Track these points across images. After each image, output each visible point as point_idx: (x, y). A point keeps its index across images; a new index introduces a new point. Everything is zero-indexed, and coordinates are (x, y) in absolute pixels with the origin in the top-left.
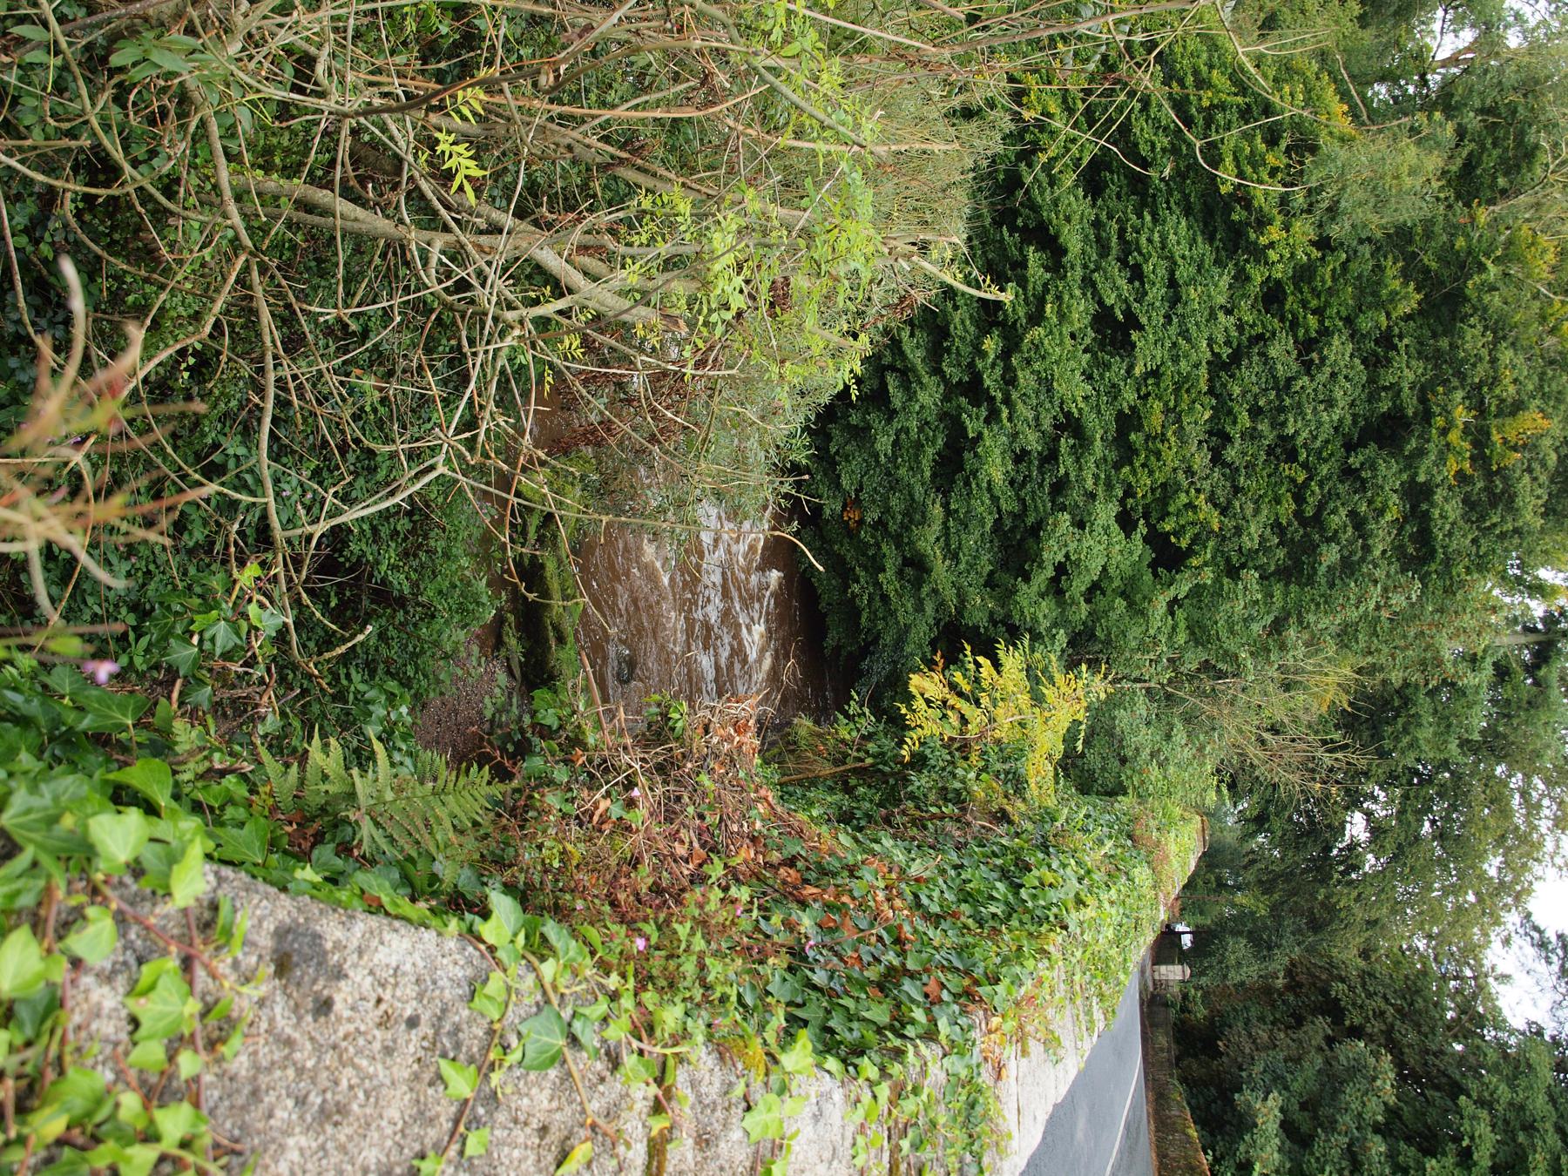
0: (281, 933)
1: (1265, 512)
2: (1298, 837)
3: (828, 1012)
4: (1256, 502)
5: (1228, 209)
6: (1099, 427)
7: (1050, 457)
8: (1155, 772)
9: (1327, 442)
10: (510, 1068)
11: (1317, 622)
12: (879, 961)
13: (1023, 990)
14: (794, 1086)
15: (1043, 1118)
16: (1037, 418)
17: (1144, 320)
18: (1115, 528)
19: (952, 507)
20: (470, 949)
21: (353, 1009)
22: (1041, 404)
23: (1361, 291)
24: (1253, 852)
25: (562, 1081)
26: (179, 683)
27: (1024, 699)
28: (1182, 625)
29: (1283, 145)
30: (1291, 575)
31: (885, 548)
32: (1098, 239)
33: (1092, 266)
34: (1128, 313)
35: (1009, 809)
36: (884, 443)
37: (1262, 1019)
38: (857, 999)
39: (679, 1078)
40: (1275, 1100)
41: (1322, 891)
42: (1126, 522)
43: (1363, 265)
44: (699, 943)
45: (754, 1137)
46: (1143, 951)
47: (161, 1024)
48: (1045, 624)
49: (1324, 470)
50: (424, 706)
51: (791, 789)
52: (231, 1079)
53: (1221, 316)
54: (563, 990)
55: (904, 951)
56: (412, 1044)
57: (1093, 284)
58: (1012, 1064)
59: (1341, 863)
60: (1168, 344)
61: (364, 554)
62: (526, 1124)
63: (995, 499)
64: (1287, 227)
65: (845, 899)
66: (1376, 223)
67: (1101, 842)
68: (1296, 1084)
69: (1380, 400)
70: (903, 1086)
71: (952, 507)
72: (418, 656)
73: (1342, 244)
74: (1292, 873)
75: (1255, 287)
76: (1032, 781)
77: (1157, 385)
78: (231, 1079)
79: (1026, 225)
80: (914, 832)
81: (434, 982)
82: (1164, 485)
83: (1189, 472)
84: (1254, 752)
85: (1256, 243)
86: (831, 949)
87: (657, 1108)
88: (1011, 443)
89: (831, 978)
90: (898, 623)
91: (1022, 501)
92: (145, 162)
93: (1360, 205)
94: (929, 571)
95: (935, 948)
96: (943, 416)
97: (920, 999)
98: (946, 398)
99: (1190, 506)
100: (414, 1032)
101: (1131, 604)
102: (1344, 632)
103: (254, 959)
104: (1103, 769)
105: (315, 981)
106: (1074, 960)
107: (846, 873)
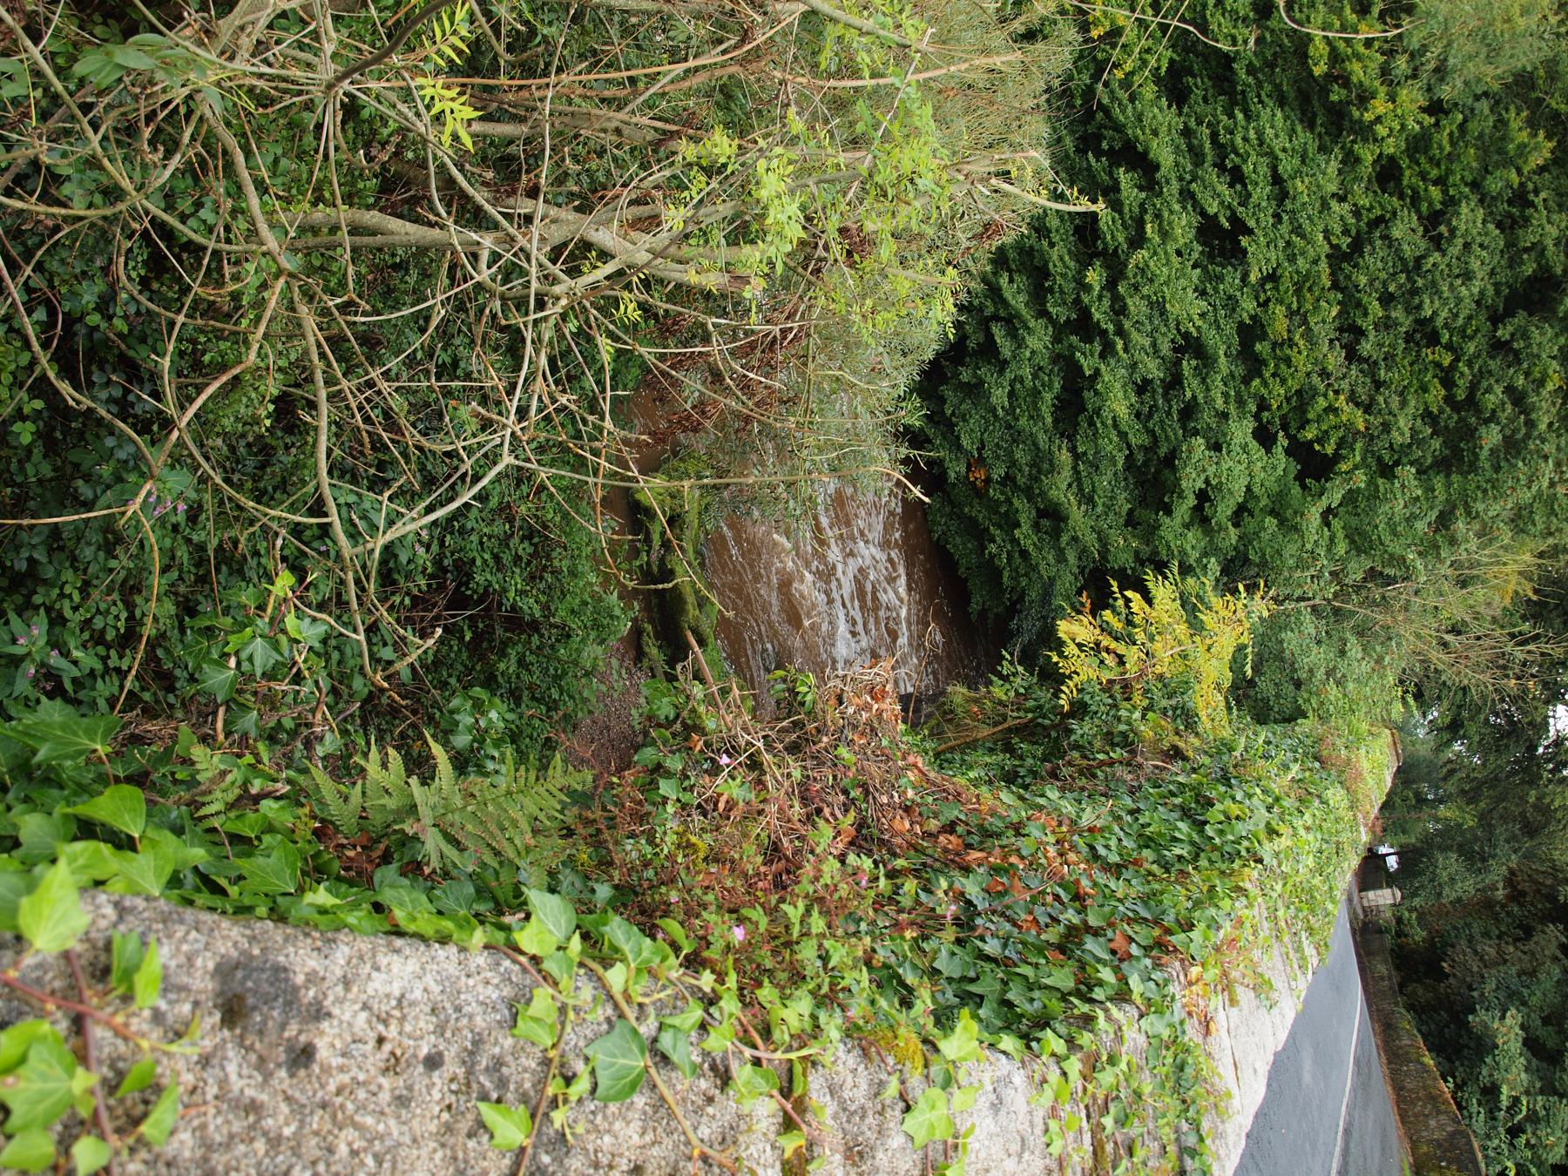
0: (224, 971)
1: (1413, 403)
2: (1498, 740)
3: (1005, 983)
4: (1401, 394)
5: (1325, 92)
6: (1220, 344)
7: (1174, 382)
8: (1333, 691)
9: (1470, 318)
10: (580, 1101)
11: (1486, 511)
12: (1058, 921)
13: (1222, 933)
14: (962, 1076)
15: (1264, 1068)
16: (1154, 345)
17: (1251, 223)
18: (1253, 445)
19: (1080, 450)
20: (507, 963)
21: (344, 1055)
22: (1156, 330)
23: (1484, 150)
24: (1450, 761)
25: (656, 1109)
26: (221, 711)
27: (1182, 629)
28: (1340, 534)
29: (1376, 11)
30: (1451, 465)
31: (1016, 501)
32: (1191, 148)
33: (1188, 177)
34: (1234, 219)
35: (1181, 745)
36: (999, 396)
37: (1486, 934)
38: (1036, 966)
39: (814, 1086)
40: (1513, 1018)
41: (1533, 792)
42: (1264, 437)
43: (1484, 121)
44: (818, 923)
45: (919, 1141)
46: (1349, 876)
47: (41, 1108)
48: (1194, 555)
49: (1471, 348)
50: (575, 727)
51: (949, 756)
52: (168, 1165)
53: (1334, 205)
54: (641, 1000)
55: (1085, 907)
56: (436, 1089)
57: (1192, 195)
58: (1221, 1015)
59: (1549, 761)
60: (1281, 244)
61: (490, 583)
62: (611, 1167)
63: (1123, 435)
64: (1392, 98)
65: (1014, 859)
66: (1491, 75)
67: (1286, 768)
68: (1534, 999)
69: (1522, 263)
70: (1097, 1057)
71: (1080, 450)
72: (561, 678)
73: (1456, 104)
74: (1496, 779)
75: (1367, 168)
76: (1203, 714)
77: (1276, 289)
78: (168, 1165)
79: (1111, 148)
80: (1083, 782)
81: (458, 1009)
82: (1299, 393)
83: (1324, 374)
84: (1437, 657)
85: (1360, 121)
86: (1003, 915)
87: (788, 1125)
88: (1131, 375)
89: (1005, 946)
90: (1041, 577)
91: (1152, 433)
92: (192, 215)
93: (1471, 58)
94: (1065, 519)
95: (1119, 900)
96: (1056, 358)
97: (1107, 957)
98: (1057, 339)
99: (1331, 409)
100: (437, 1073)
101: (1282, 522)
102: (1519, 516)
103: (186, 1008)
104: (1278, 696)
105: (283, 1026)
106: (1275, 895)
107: (1011, 833)
